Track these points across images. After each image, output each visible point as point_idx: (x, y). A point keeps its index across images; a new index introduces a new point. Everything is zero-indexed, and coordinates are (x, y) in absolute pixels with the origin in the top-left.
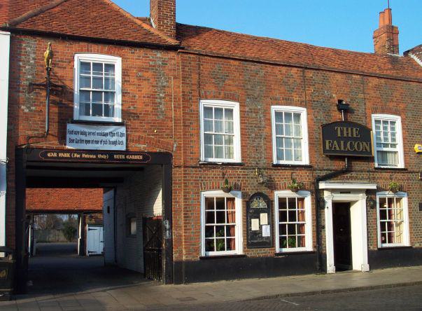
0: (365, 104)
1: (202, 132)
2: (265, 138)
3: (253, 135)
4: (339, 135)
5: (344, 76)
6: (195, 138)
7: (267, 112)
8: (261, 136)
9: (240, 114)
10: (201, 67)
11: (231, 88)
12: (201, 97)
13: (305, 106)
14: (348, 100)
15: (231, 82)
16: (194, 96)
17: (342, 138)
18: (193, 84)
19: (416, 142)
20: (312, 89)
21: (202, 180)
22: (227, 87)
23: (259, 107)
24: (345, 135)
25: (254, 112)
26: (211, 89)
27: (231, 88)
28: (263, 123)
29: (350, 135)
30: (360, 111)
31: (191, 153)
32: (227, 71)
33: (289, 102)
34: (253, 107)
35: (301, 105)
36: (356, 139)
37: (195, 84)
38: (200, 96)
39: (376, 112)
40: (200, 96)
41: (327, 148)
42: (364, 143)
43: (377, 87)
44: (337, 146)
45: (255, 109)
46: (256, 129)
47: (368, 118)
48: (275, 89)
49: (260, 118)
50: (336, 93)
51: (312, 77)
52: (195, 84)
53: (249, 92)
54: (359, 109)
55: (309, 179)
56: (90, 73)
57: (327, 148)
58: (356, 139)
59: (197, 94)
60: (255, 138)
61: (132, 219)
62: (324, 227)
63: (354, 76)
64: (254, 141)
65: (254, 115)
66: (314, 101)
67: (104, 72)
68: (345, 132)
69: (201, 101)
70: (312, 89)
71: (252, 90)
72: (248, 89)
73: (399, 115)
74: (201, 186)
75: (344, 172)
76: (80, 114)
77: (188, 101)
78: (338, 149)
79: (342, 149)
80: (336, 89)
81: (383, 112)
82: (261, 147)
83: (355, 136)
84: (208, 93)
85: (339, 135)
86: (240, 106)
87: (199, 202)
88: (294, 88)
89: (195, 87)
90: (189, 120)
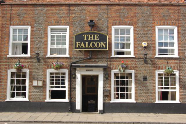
0: (108, 21)
1: (11, 41)
2: (43, 43)
3: (37, 42)
4: (85, 39)
5: (95, 7)
6: (7, 44)
7: (46, 30)
8: (42, 41)
9: (31, 32)
10: (12, 10)
11: (27, 19)
12: (10, 25)
13: (69, 25)
14: (97, 19)
15: (27, 17)
16: (7, 25)
17: (87, 41)
18: (7, 19)
19: (144, 41)
20: (74, 15)
21: (9, 64)
22: (25, 19)
23: (41, 27)
24: (89, 39)
25: (38, 30)
26: (17, 21)
27: (27, 19)
28: (43, 35)
29: (92, 39)
30: (104, 25)
31: (5, 52)
32: (26, 11)
33: (58, 23)
34: (39, 27)
35: (66, 25)
36: (96, 41)
37: (8, 19)
38: (10, 24)
39: (115, 24)
40: (10, 24)
41: (77, 47)
42: (102, 43)
43: (117, 11)
44: (83, 45)
45: (39, 29)
46: (39, 38)
47: (109, 29)
48: (51, 18)
49: (42, 33)
50: (89, 17)
51: (74, 9)
52: (8, 19)
53: (37, 20)
54: (102, 24)
55: (68, 63)
56: (55, 40)
57: (77, 47)
58: (96, 41)
59: (9, 24)
60: (38, 43)
61: (78, 69)
62: (75, 88)
63: (152, 60)
64: (37, 45)
65: (38, 32)
66: (74, 22)
67: (56, 39)
68: (92, 37)
69: (11, 27)
70: (74, 15)
71: (38, 19)
72: (36, 19)
73: (132, 25)
74: (8, 67)
75: (90, 59)
76: (115, 55)
77: (4, 27)
78: (84, 47)
79: (87, 46)
80: (88, 14)
81: (120, 24)
82: (41, 47)
83: (96, 39)
84: (15, 23)
85: (85, 39)
86: (31, 27)
87: (7, 74)
88: (62, 16)
89: (8, 20)
90: (4, 36)
